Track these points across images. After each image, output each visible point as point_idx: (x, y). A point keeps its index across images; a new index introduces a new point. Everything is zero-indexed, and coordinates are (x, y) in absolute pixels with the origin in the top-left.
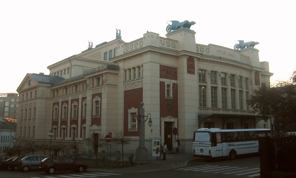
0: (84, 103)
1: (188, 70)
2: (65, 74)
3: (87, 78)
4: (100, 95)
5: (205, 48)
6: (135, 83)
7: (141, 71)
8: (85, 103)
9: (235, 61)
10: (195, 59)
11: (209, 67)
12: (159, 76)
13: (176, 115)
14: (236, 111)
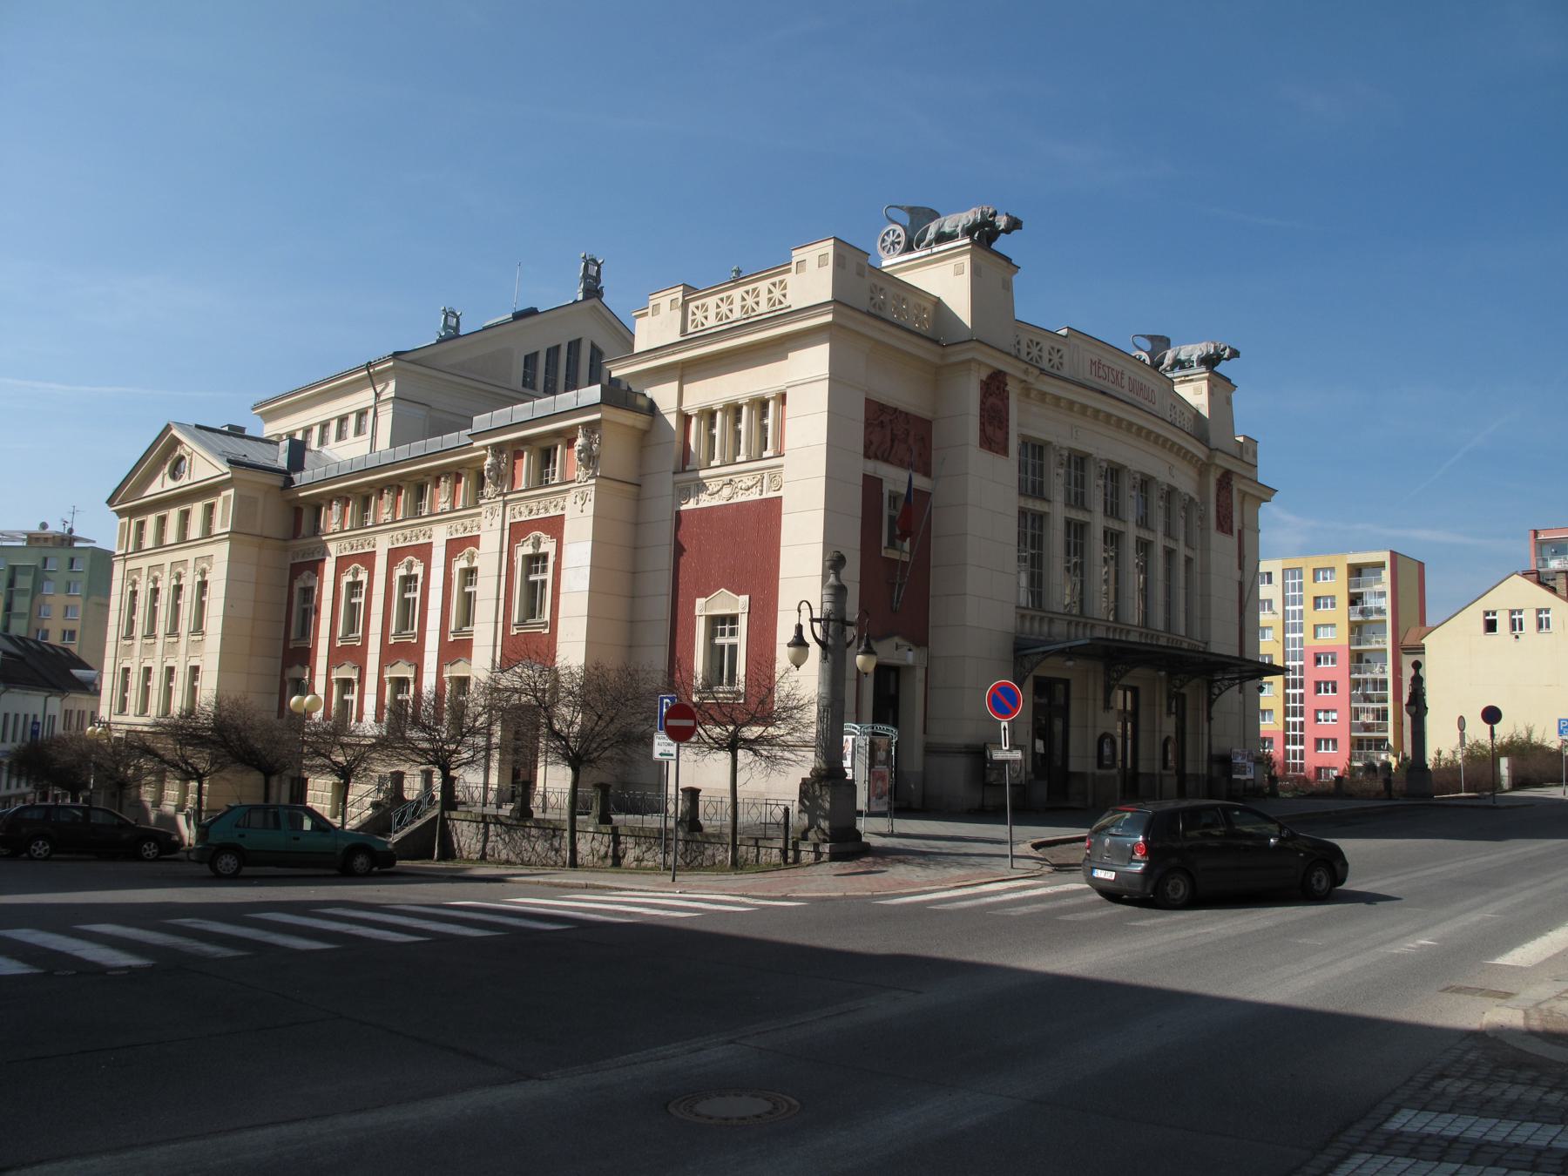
0: (460, 564)
1: (983, 430)
2: (340, 436)
3: (485, 447)
4: (554, 526)
6: (736, 478)
7: (769, 421)
9: (1104, 393)
10: (1009, 381)
11: (1058, 431)
12: (861, 450)
13: (919, 638)
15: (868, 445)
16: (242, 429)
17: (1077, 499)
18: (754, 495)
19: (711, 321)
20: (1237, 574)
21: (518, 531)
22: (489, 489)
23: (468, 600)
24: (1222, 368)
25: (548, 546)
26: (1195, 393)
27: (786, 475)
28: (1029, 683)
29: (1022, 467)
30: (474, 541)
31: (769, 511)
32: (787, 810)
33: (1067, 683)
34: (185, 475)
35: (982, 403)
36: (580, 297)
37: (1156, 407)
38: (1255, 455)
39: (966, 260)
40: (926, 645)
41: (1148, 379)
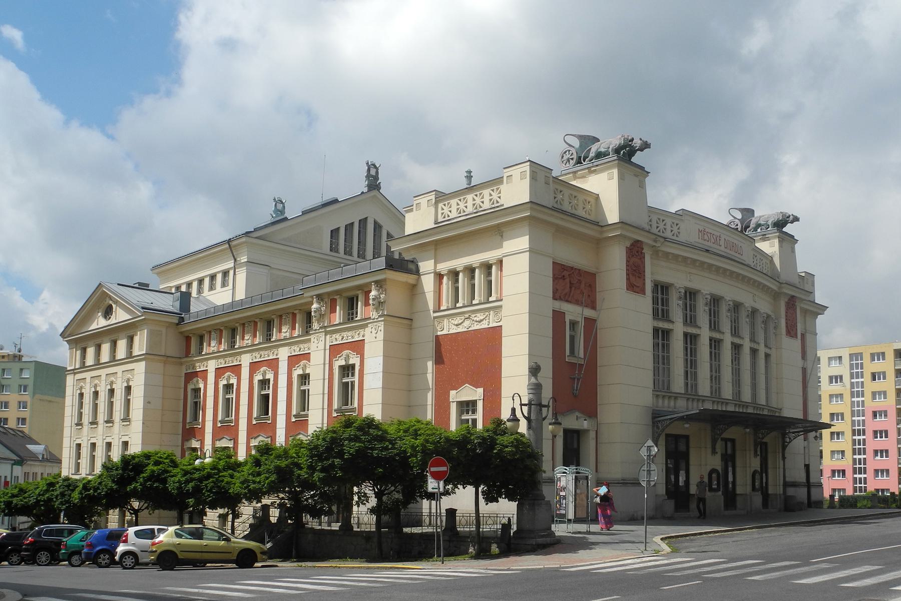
1: (628, 279)
2: (212, 287)
4: (358, 347)
5: (669, 222)
8: (300, 372)
9: (707, 251)
11: (680, 279)
13: (591, 413)
14: (670, 397)
15: (555, 292)
16: (147, 285)
17: (691, 320)
18: (484, 325)
19: (454, 214)
20: (800, 363)
21: (335, 350)
22: (315, 325)
23: (304, 396)
24: (788, 229)
25: (354, 360)
26: (770, 247)
27: (504, 312)
28: (662, 441)
29: (655, 301)
30: (307, 356)
31: (496, 332)
32: (509, 519)
33: (687, 437)
34: (113, 317)
35: (627, 261)
36: (365, 190)
37: (743, 257)
38: (813, 285)
39: (615, 172)
40: (596, 416)
41: (736, 239)
